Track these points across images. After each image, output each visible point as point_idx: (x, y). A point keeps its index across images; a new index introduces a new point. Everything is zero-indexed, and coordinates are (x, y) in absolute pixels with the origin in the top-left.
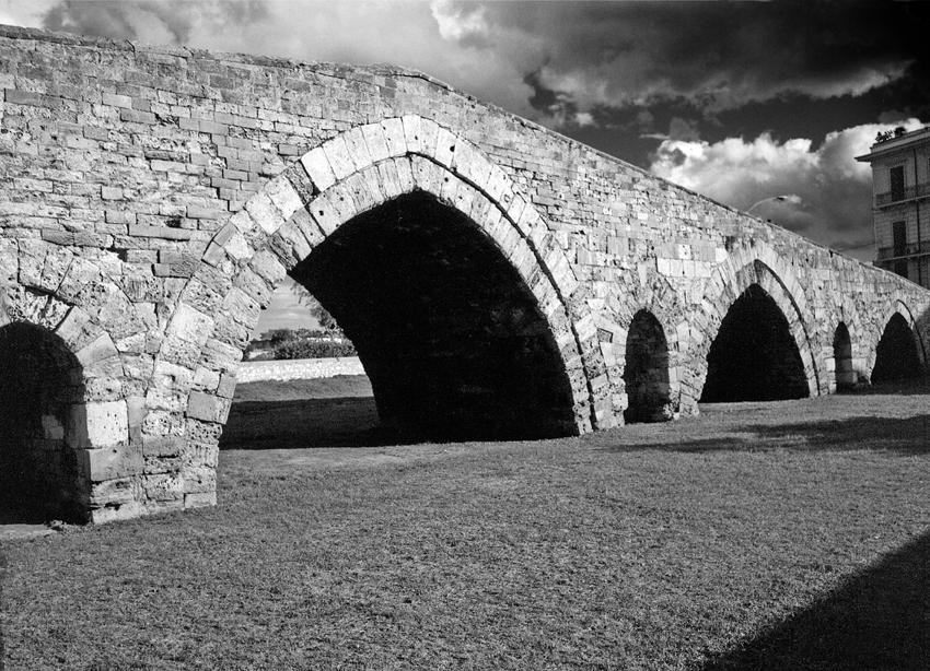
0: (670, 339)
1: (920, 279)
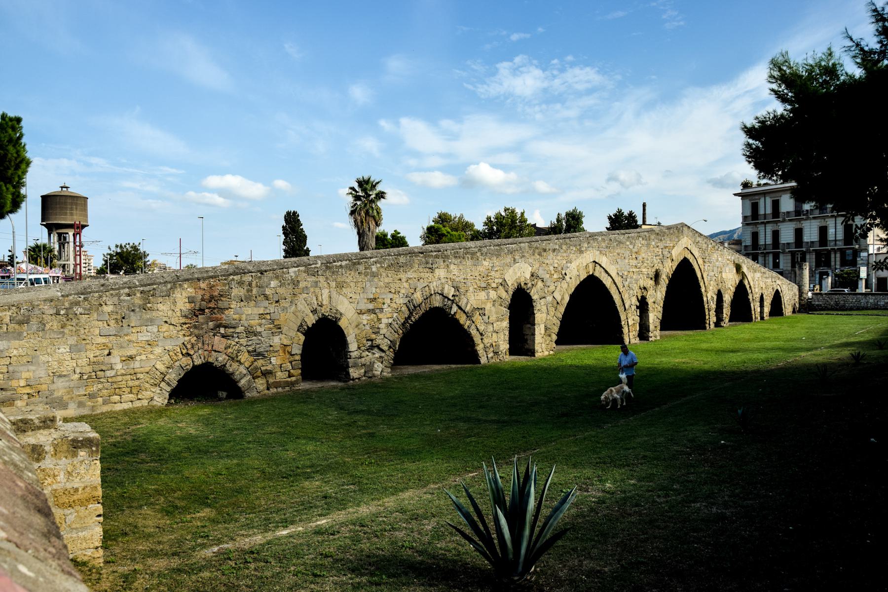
0: (724, 299)
1: (765, 264)
